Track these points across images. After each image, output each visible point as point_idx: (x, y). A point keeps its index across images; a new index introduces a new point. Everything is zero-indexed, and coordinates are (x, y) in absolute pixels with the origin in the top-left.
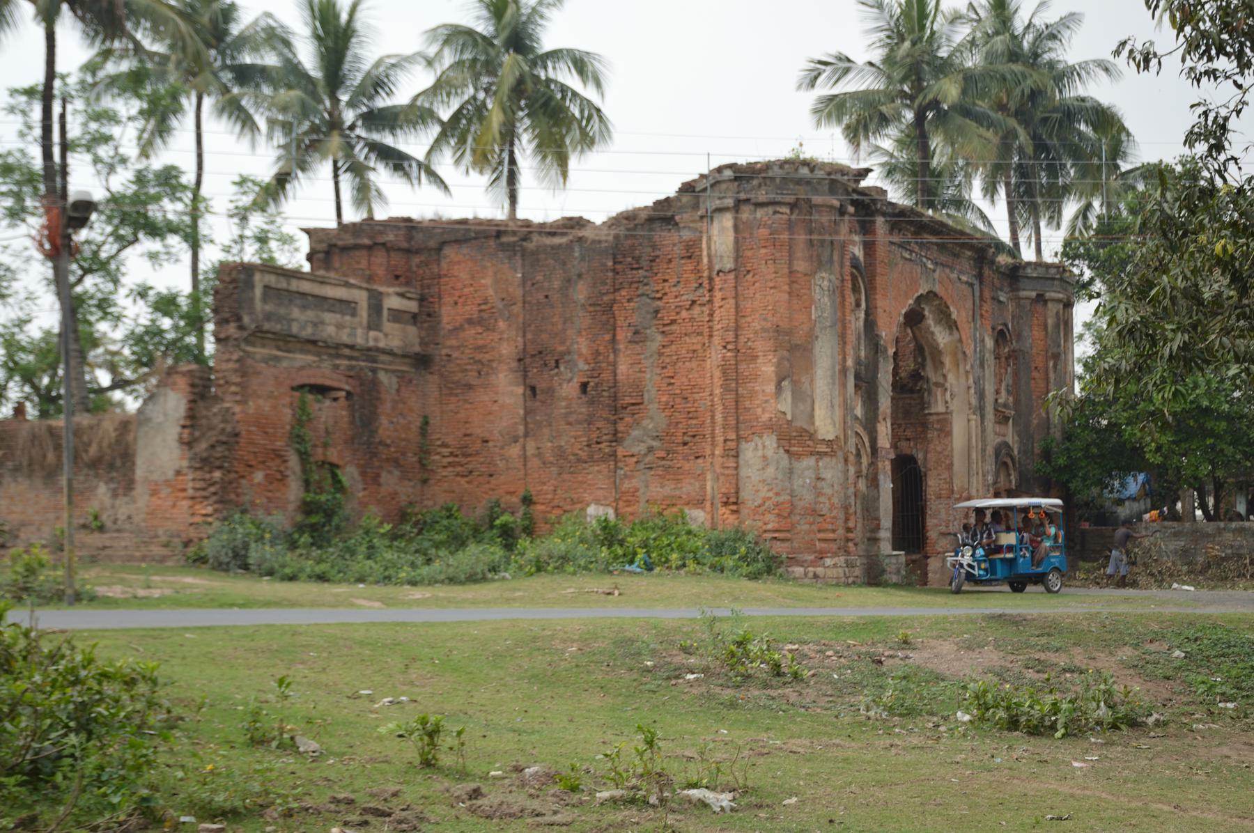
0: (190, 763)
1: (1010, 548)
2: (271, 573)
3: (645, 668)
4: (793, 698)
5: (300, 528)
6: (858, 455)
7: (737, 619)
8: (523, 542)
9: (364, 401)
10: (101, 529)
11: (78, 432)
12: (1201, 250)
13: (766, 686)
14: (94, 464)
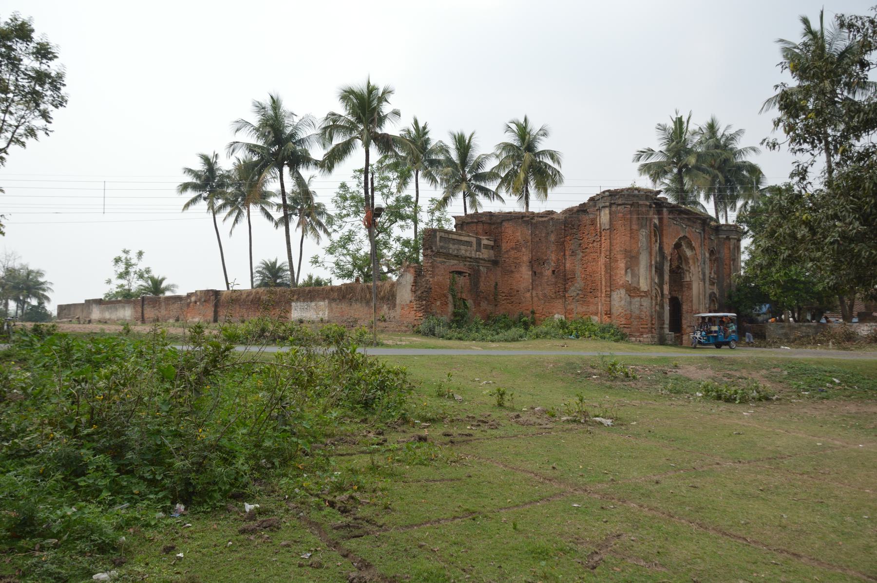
0: (418, 402)
1: (715, 332)
2: (442, 337)
3: (577, 373)
4: (633, 385)
5: (453, 321)
6: (656, 297)
7: (612, 356)
8: (532, 327)
9: (475, 277)
10: (385, 321)
11: (377, 287)
12: (797, 218)
13: (623, 381)
14: (382, 298)
